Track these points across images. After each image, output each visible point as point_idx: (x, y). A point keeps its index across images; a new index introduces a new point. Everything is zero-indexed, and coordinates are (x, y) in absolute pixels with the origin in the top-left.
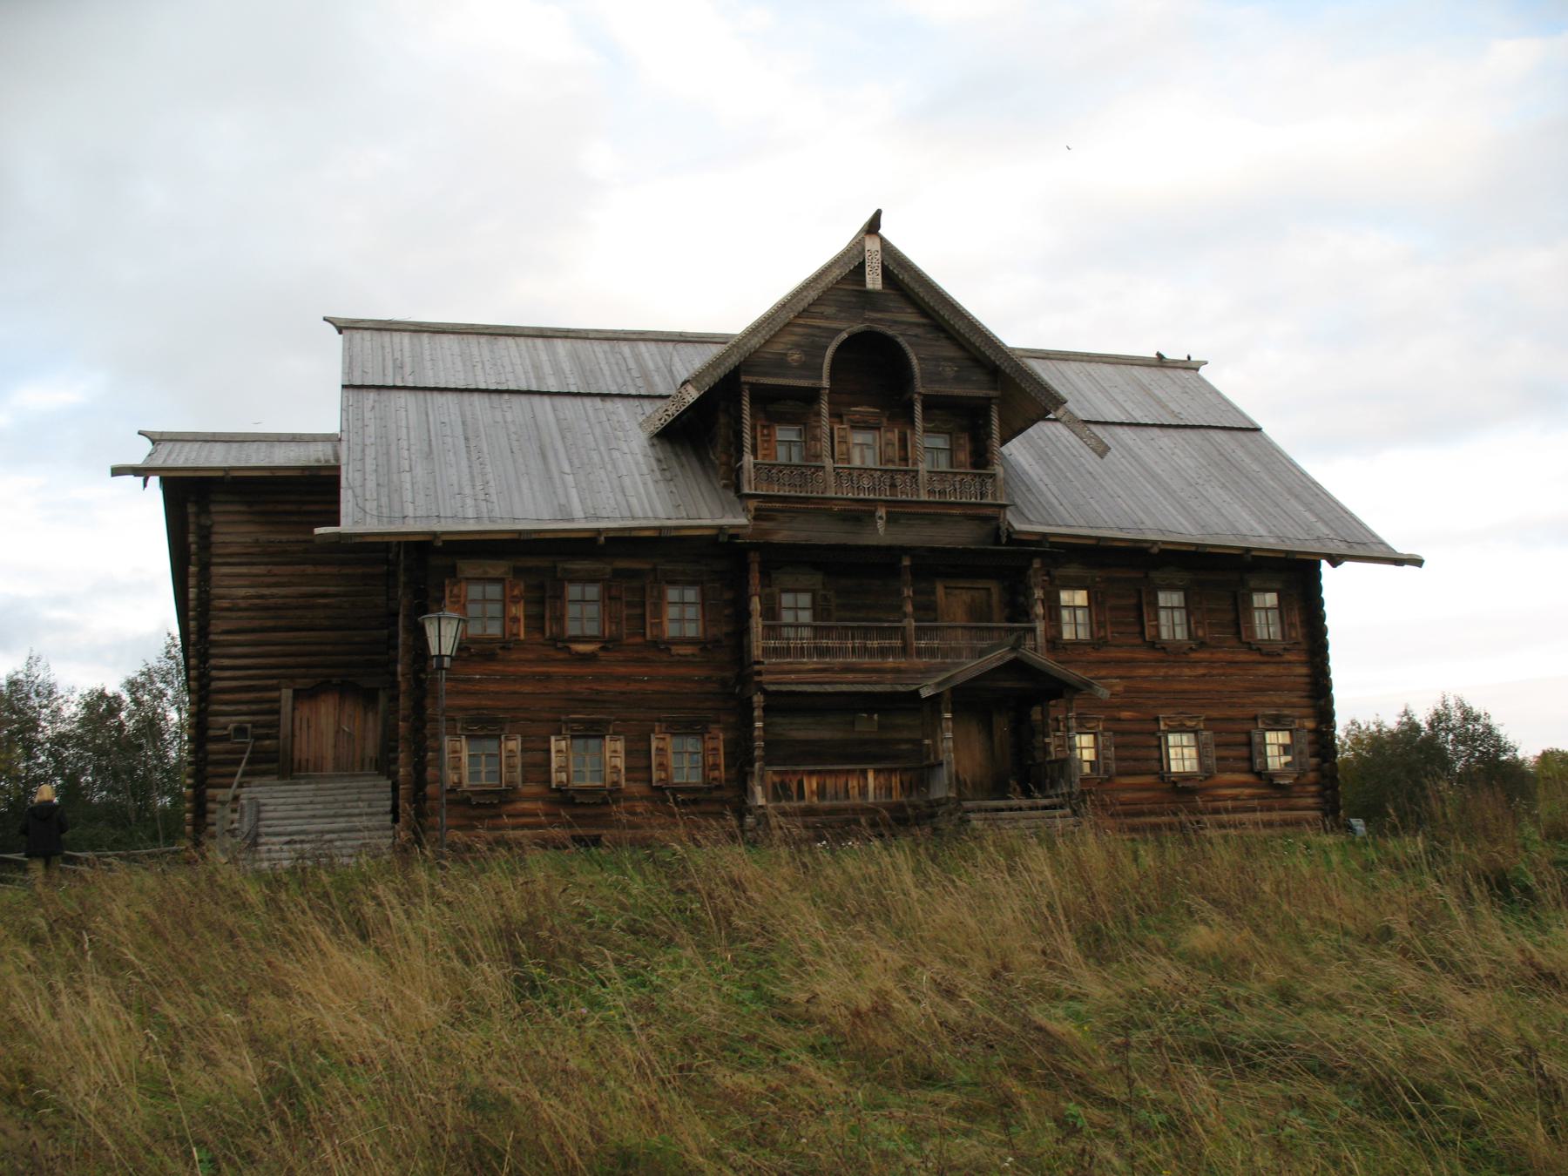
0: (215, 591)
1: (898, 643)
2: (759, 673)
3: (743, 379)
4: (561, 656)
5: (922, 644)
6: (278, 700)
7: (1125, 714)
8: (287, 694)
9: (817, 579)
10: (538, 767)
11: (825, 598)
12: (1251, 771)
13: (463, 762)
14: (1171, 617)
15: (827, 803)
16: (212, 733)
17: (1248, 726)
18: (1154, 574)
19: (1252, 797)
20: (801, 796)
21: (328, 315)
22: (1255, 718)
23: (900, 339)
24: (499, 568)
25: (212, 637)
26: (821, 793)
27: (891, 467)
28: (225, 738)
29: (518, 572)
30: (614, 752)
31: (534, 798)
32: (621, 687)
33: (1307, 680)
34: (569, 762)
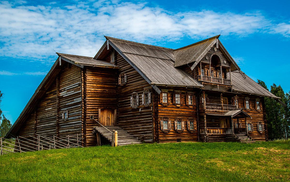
1: (221, 108)
6: (98, 111)
8: (100, 110)
12: (257, 131)
14: (178, 99)
17: (256, 123)
19: (257, 135)
21: (105, 36)
22: (257, 122)
25: (87, 98)
27: (215, 77)
28: (89, 118)
29: (169, 92)
31: (172, 132)
33: (263, 116)
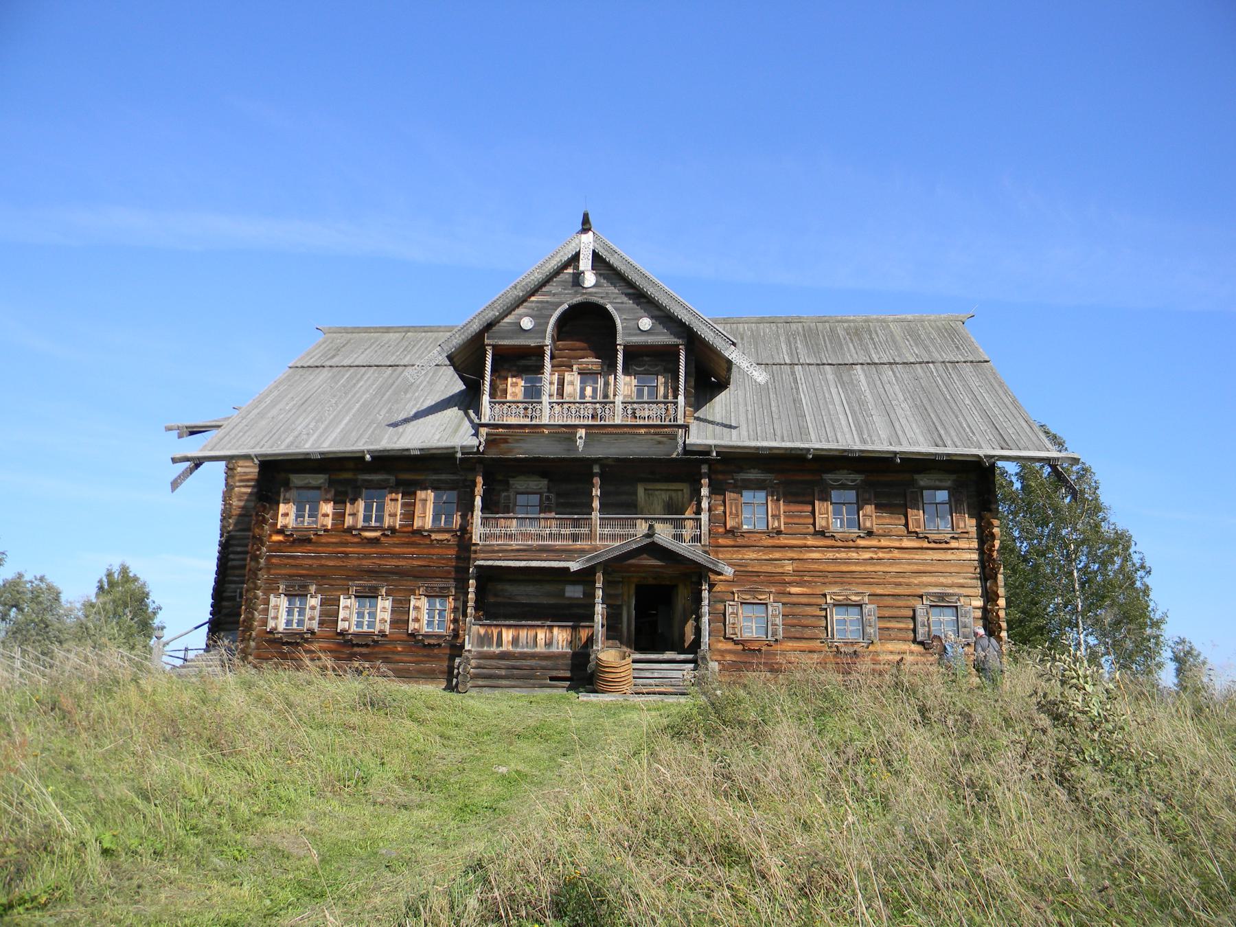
0: (975, 556)
2: (475, 552)
3: (486, 341)
4: (356, 540)
5: (606, 531)
7: (794, 590)
9: (543, 484)
10: (329, 616)
11: (548, 498)
13: (280, 613)
15: (519, 650)
16: (226, 594)
18: (828, 477)
20: (500, 644)
23: (609, 307)
24: (320, 479)
26: (515, 641)
30: (384, 606)
32: (394, 562)
34: (351, 615)
